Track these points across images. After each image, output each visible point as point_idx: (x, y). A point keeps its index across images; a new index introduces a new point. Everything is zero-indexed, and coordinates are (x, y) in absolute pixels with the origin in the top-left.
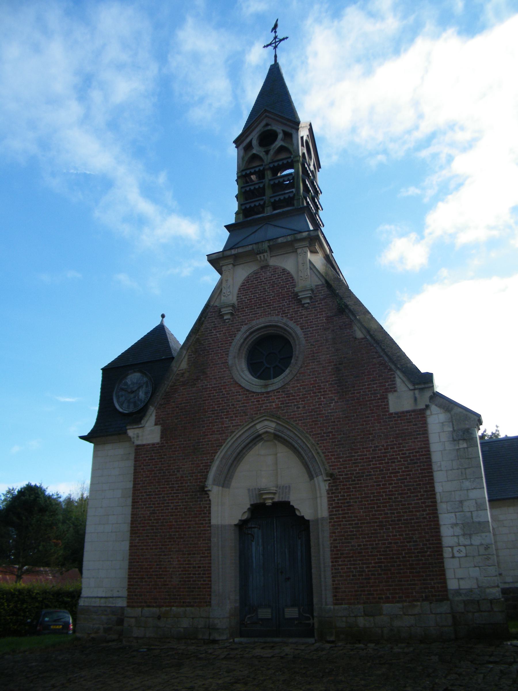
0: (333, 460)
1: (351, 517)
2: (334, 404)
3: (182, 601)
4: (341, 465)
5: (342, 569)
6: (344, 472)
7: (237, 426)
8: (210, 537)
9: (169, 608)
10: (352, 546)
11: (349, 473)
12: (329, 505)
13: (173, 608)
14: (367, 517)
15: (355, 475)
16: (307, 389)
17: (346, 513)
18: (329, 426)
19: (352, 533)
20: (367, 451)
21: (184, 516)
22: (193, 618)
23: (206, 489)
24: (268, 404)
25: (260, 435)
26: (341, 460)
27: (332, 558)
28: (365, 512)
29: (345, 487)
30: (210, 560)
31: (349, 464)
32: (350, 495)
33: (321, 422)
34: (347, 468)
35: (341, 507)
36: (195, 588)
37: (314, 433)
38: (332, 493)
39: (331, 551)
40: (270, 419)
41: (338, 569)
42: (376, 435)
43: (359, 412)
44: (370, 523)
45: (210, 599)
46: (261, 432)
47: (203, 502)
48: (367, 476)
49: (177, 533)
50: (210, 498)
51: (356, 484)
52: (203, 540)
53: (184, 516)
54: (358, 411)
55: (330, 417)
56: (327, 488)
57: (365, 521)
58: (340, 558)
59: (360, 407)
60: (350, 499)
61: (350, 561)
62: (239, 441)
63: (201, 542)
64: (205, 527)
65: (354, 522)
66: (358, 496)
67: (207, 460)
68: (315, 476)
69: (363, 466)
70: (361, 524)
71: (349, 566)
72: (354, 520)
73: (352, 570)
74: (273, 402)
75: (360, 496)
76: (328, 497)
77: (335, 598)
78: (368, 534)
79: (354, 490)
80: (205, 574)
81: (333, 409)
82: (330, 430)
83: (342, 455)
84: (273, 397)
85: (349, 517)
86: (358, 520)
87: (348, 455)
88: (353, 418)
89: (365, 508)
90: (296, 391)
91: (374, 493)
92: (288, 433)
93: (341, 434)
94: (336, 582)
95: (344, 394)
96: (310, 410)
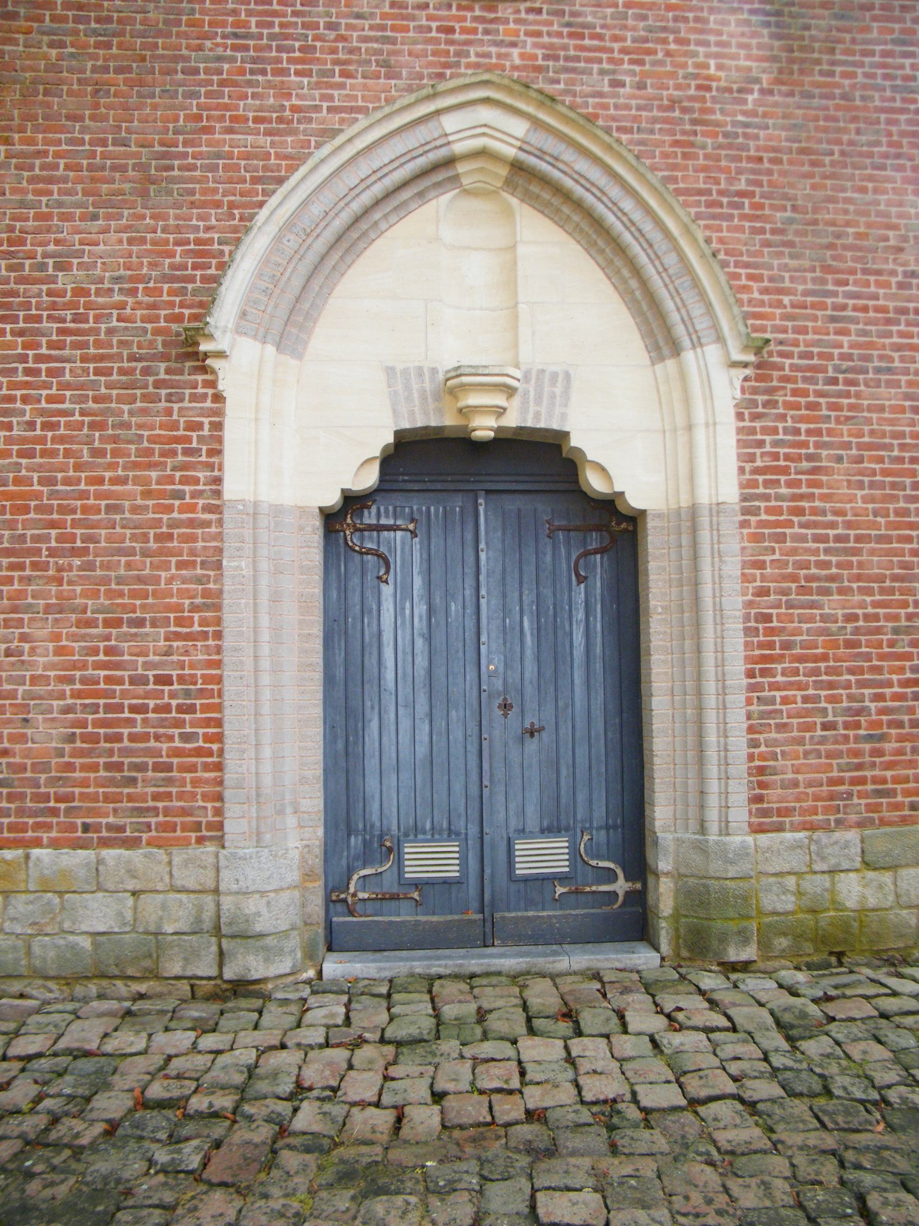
0: (756, 295)
1: (823, 513)
2: (756, 95)
3: (79, 821)
4: (785, 317)
5: (785, 701)
6: (796, 344)
7: (352, 110)
8: (220, 551)
9: (20, 852)
10: (824, 618)
11: (816, 350)
12: (740, 456)
13: (36, 852)
14: (879, 519)
15: (837, 362)
16: (650, 22)
17: (801, 497)
18: (740, 172)
19: (824, 572)
20: (879, 284)
21: (86, 458)
22: (134, 893)
23: (204, 347)
24: (493, 50)
25: (450, 162)
26: (786, 300)
27: (748, 659)
28: (872, 500)
29: (802, 400)
30: (219, 650)
31: (815, 318)
32: (819, 432)
33: (709, 150)
34: (807, 333)
35: (785, 471)
36: (142, 768)
37: (681, 185)
38: (755, 417)
39: (748, 631)
40: (509, 100)
41: (772, 701)
42: (911, 234)
43: (851, 143)
44: (888, 539)
45: (219, 812)
46: (459, 148)
47: (186, 404)
48: (878, 370)
49: (54, 532)
50: (220, 387)
51: (840, 395)
52: (181, 565)
53: (86, 458)
54: (845, 138)
55: (740, 140)
56: (738, 394)
57: (873, 533)
58: (780, 659)
59: (852, 126)
60: (817, 445)
61: (816, 672)
62: (364, 168)
63: (173, 571)
64: (192, 508)
65: (831, 532)
66: (846, 439)
67: (208, 229)
68: (686, 342)
69: (865, 333)
70: (858, 539)
71: (811, 692)
72: (833, 525)
73: (823, 705)
74: (514, 45)
75: (854, 440)
76: (740, 430)
77: (754, 807)
78: (881, 579)
79: (833, 414)
80: (191, 709)
81: (754, 114)
82: (742, 186)
83: (787, 284)
84: (512, 26)
85: (814, 511)
86: (849, 525)
87: (810, 286)
88: (827, 159)
89: (872, 485)
90: (609, 21)
91: (902, 435)
92: (582, 165)
93: (784, 209)
94: (763, 748)
95: (796, 67)
96: (665, 102)
